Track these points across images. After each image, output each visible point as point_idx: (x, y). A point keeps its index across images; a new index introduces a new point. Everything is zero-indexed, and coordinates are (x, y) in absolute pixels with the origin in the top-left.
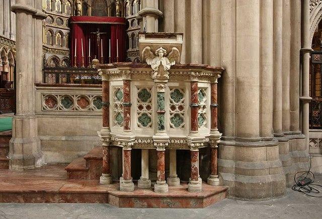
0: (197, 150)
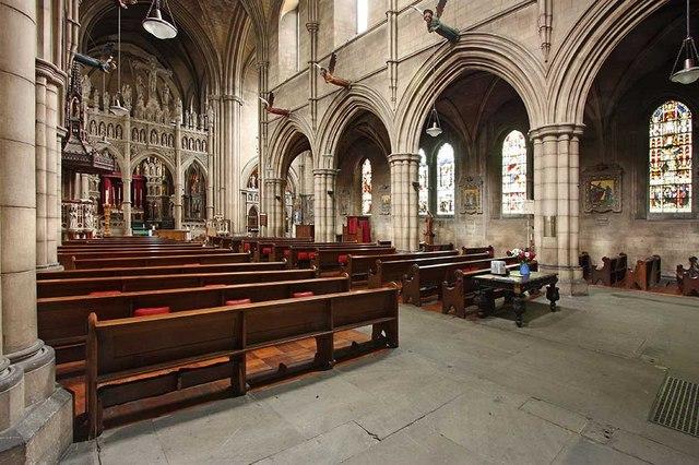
0: (227, 232)
